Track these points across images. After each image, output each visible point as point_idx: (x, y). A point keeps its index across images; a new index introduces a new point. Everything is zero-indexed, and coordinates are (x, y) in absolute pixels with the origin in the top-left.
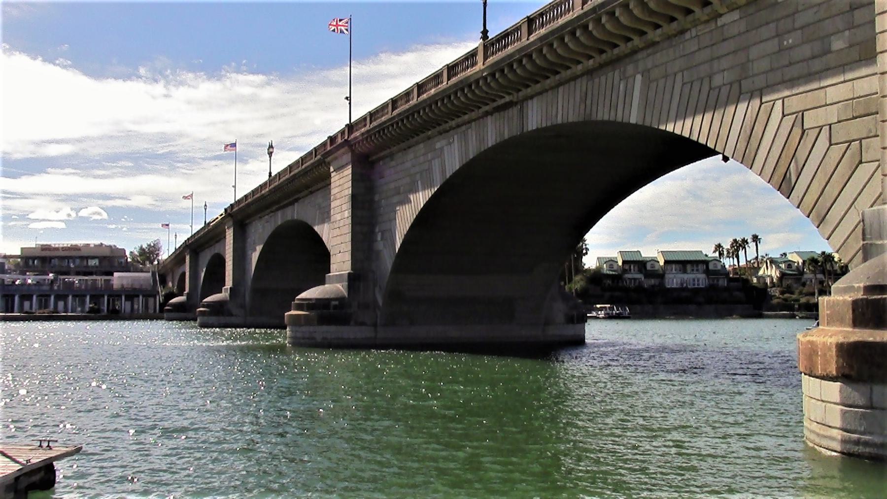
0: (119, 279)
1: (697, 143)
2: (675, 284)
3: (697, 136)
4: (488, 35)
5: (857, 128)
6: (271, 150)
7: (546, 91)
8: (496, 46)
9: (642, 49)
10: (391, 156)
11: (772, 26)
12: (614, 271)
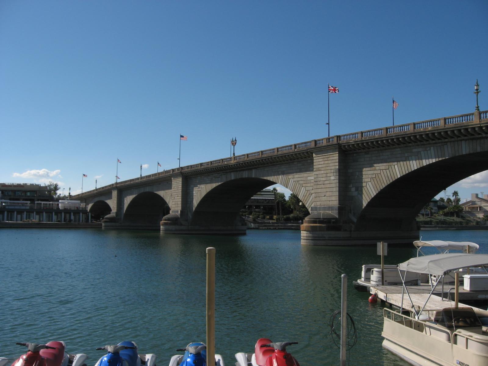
1: (272, 182)
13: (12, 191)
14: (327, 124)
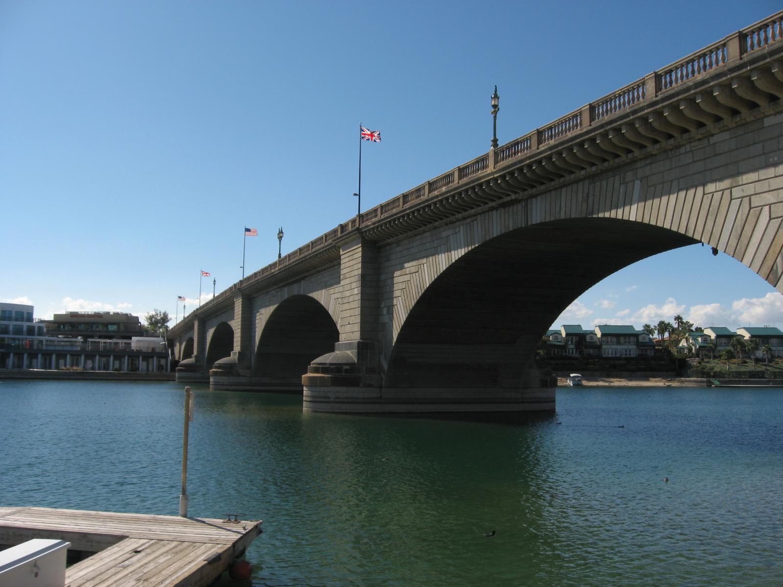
0: (136, 342)
3: (692, 233)
7: (550, 191)
8: (506, 152)
9: (641, 159)
10: (398, 243)
13: (86, 323)
14: (355, 195)
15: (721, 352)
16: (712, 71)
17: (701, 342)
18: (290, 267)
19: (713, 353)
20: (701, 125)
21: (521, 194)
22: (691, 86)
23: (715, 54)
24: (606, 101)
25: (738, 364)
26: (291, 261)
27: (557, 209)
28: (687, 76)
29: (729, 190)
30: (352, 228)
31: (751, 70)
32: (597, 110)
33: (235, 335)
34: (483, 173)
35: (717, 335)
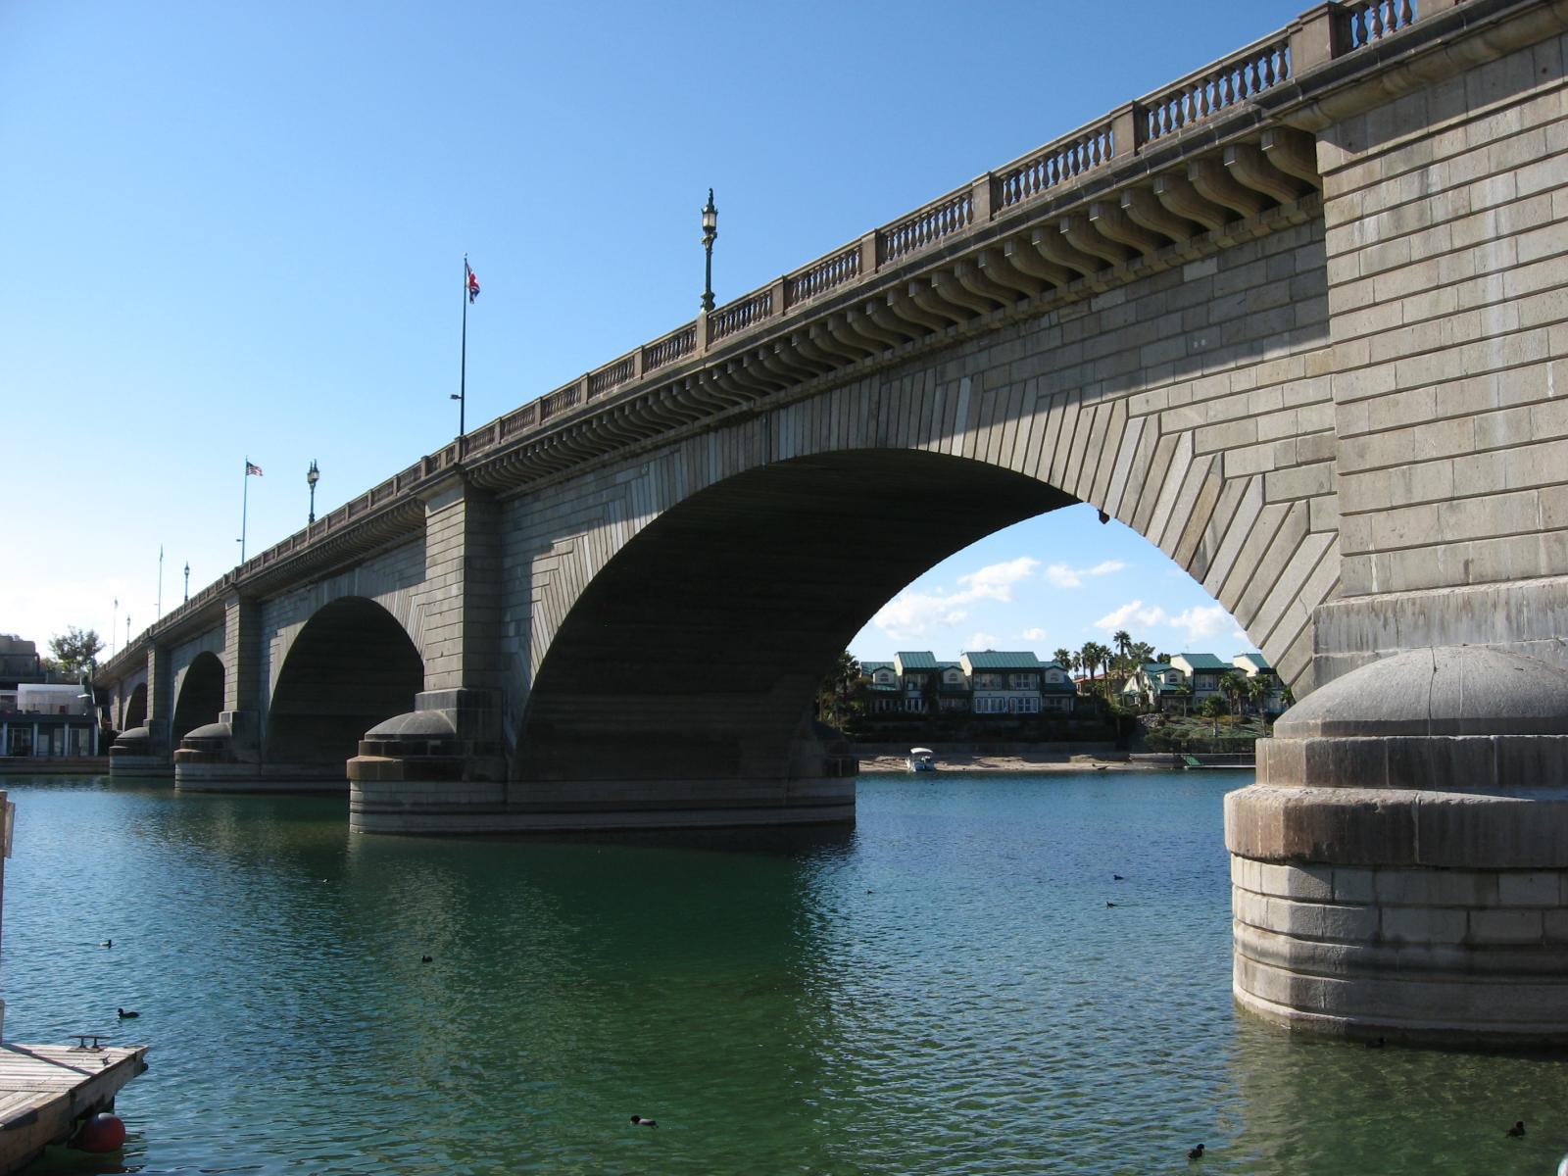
0: (26, 695)
2: (989, 709)
4: (714, 301)
5: (1303, 481)
6: (315, 475)
7: (812, 396)
8: (729, 320)
9: (971, 339)
10: (536, 494)
11: (1176, 318)
12: (889, 685)
14: (454, 397)
15: (1203, 702)
16: (1087, 175)
17: (1166, 684)
18: (332, 541)
19: (1187, 704)
20: (1074, 276)
21: (759, 401)
22: (1051, 201)
23: (1094, 143)
24: (905, 225)
25: (1236, 725)
26: (333, 529)
27: (825, 432)
28: (1217, 104)
29: (1124, 400)
30: (447, 463)
31: (1154, 176)
32: (1005, 187)
33: (227, 680)
34: (686, 359)
35: (1260, 669)
